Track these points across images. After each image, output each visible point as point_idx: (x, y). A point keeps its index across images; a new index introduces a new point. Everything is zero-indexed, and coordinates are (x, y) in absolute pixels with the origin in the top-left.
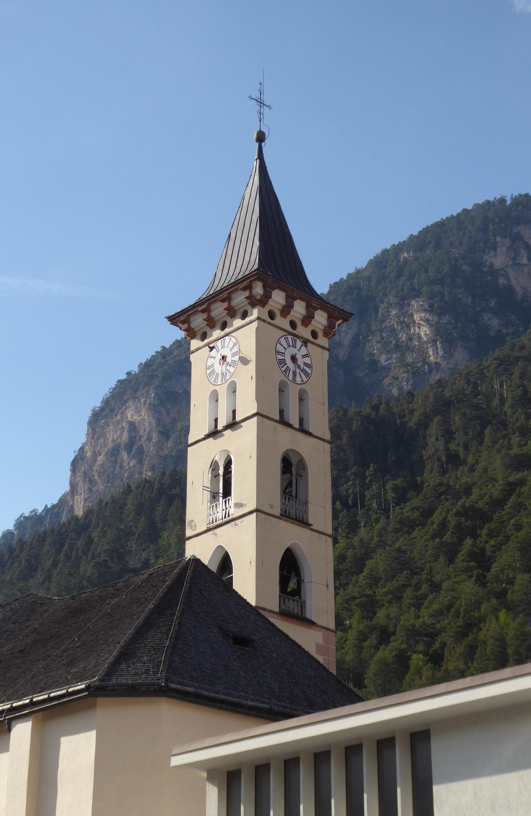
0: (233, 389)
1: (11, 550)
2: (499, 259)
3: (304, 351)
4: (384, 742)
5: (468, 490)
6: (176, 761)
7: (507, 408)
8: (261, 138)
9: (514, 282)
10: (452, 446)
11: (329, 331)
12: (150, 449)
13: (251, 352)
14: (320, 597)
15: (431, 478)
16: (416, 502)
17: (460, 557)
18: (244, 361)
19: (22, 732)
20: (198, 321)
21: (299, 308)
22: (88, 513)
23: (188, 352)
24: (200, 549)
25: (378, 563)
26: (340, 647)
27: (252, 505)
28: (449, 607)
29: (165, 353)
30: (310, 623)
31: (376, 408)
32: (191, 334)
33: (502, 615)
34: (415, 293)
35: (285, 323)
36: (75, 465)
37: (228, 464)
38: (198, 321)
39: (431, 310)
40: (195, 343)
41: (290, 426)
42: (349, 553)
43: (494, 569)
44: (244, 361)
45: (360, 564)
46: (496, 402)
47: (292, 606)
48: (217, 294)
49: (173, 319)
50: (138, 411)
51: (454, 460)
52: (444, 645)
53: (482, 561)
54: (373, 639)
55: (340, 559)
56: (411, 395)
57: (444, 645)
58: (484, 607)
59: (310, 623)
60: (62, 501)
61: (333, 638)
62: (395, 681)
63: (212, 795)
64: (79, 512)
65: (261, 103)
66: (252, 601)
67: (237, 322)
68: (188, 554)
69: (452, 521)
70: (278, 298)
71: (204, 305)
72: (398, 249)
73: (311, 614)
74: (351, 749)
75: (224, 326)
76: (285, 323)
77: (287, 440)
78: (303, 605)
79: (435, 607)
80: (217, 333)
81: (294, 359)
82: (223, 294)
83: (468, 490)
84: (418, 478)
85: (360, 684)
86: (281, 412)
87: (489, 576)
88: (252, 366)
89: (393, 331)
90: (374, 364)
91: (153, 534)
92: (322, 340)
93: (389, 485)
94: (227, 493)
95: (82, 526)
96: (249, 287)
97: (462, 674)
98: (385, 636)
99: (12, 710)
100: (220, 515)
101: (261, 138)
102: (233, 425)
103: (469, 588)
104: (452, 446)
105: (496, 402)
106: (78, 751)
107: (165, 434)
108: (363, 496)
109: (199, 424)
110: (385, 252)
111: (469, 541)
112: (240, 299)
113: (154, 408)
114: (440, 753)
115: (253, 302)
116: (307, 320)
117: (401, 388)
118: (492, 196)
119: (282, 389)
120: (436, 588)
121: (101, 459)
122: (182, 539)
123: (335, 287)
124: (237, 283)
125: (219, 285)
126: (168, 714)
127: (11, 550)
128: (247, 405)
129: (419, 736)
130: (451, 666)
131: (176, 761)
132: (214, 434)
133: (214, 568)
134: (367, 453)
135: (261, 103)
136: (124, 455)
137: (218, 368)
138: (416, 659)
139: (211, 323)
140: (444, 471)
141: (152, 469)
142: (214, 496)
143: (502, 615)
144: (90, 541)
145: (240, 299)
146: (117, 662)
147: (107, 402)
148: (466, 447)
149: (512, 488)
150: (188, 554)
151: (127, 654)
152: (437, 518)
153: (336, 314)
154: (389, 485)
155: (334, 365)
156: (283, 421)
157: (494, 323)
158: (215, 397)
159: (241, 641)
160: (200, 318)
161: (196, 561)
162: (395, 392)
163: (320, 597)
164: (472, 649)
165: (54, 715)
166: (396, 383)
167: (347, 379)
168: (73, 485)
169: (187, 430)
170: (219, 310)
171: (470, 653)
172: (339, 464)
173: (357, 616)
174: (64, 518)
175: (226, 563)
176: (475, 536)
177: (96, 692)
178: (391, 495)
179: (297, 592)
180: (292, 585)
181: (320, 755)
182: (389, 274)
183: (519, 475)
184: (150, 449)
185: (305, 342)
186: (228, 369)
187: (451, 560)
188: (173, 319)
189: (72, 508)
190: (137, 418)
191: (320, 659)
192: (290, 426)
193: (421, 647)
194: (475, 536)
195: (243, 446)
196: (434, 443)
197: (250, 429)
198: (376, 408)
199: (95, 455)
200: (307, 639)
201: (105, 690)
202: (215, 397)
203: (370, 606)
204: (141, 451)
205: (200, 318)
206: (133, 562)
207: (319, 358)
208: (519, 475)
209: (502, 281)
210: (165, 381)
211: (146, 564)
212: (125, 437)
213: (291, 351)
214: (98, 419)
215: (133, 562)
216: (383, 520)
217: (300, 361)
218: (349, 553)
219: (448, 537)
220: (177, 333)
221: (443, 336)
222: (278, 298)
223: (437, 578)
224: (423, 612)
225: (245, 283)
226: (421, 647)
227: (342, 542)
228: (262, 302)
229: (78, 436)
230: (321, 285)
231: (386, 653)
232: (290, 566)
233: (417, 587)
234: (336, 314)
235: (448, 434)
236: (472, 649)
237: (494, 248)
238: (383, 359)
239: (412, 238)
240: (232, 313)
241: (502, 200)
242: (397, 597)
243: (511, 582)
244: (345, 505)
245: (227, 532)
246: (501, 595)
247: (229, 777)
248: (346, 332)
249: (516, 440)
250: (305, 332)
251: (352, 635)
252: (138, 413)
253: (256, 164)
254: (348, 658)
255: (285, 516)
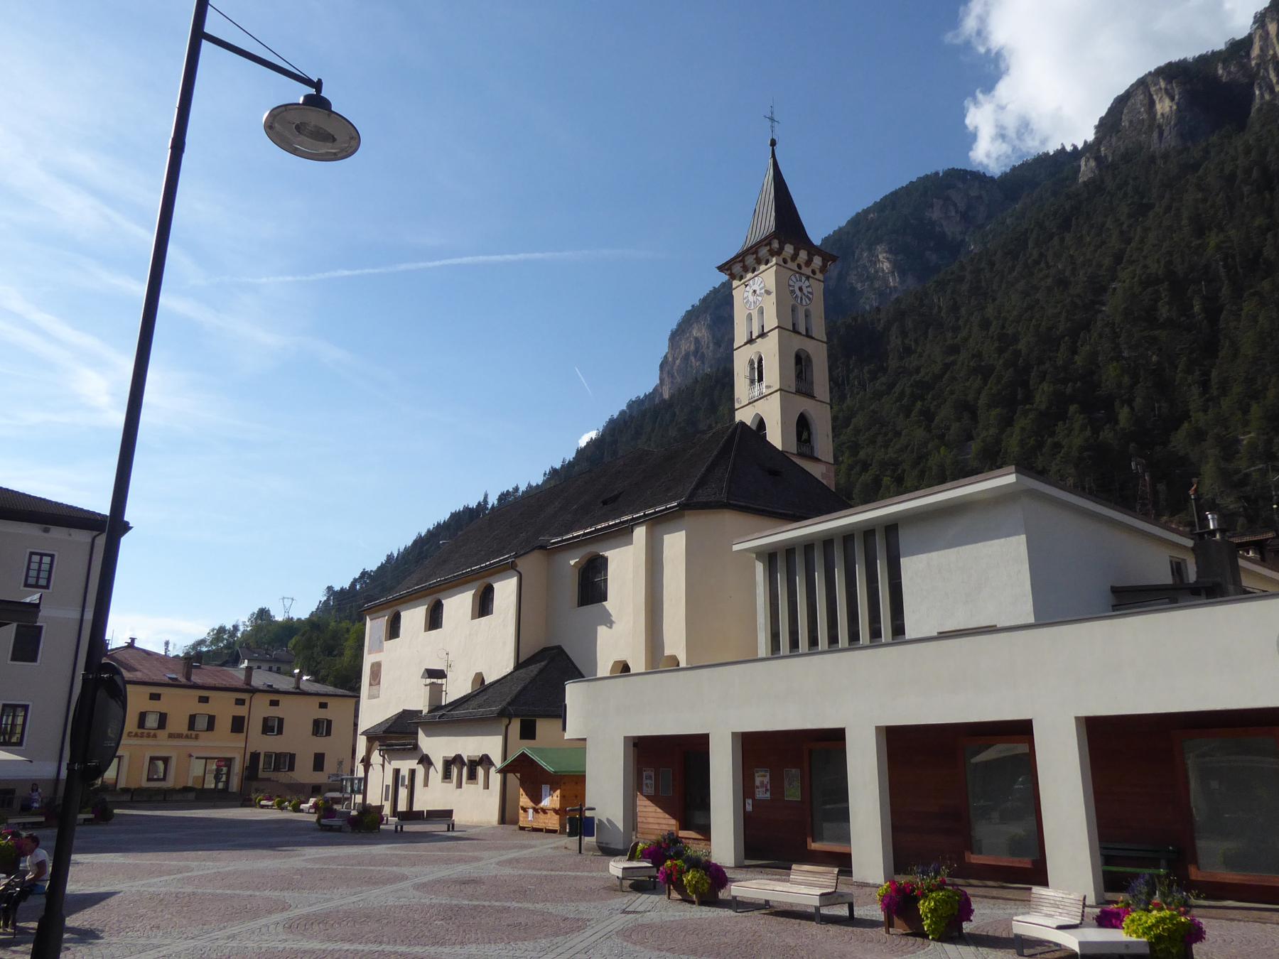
0: (761, 311)
1: (625, 422)
2: (935, 214)
3: (807, 283)
4: (868, 532)
5: (918, 370)
6: (735, 548)
7: (942, 314)
8: (773, 143)
9: (946, 230)
10: (907, 341)
11: (823, 269)
12: (709, 353)
13: (773, 288)
14: (824, 443)
15: (893, 363)
16: (883, 379)
17: (913, 414)
18: (768, 293)
19: (640, 533)
20: (737, 269)
21: (803, 255)
22: (672, 397)
23: (731, 289)
24: (744, 416)
25: (859, 420)
26: (837, 474)
27: (778, 387)
28: (907, 447)
29: (715, 291)
30: (817, 460)
31: (855, 319)
32: (733, 277)
33: (942, 450)
34: (879, 241)
35: (794, 266)
36: (662, 366)
37: (760, 360)
38: (737, 269)
39: (890, 251)
40: (735, 283)
41: (799, 333)
42: (841, 415)
43: (937, 419)
44: (768, 293)
45: (847, 422)
46: (935, 310)
47: (805, 449)
48: (748, 250)
49: (721, 268)
50: (700, 330)
51: (908, 351)
52: (904, 471)
53: (928, 416)
54: (858, 468)
55: (834, 419)
56: (878, 310)
57: (904, 471)
58: (930, 446)
59: (817, 460)
60: (655, 390)
61: (833, 468)
62: (873, 495)
63: (760, 568)
64: (666, 396)
65: (772, 120)
66: (780, 448)
67: (763, 267)
68: (737, 419)
69: (908, 391)
70: (789, 249)
71: (740, 258)
72: (867, 212)
73: (818, 454)
74: (847, 537)
75: (754, 271)
76: (794, 266)
77: (798, 343)
78: (812, 448)
79: (898, 447)
80: (750, 275)
81: (801, 289)
82: (753, 250)
83: (918, 370)
84: (36, 805)
85: (850, 498)
86: (794, 325)
87: (933, 426)
88: (774, 295)
89: (865, 267)
90: (853, 290)
91: (713, 408)
92: (819, 276)
93: (866, 369)
94: (760, 379)
95: (668, 405)
96: (770, 244)
97: (917, 489)
98: (865, 466)
99: (633, 519)
100: (756, 393)
101: (773, 143)
102: (763, 335)
103: (920, 433)
104: (907, 341)
105: (935, 310)
106: (675, 543)
107: (718, 344)
108: (848, 377)
109: (740, 336)
110: (858, 214)
111: (919, 404)
112: (764, 251)
113: (710, 328)
114: (905, 537)
115: (772, 253)
116: (809, 263)
117: (871, 306)
118: (929, 171)
119: (794, 309)
120: (898, 434)
121: (678, 362)
122: (732, 411)
123: (825, 240)
124: (761, 241)
125: (749, 244)
126: (729, 520)
127: (625, 422)
128: (771, 321)
129: (891, 528)
130: (909, 485)
131: (735, 548)
132: (751, 341)
133: (754, 427)
134: (851, 348)
135: (772, 120)
136: (692, 359)
137: (751, 298)
138: (886, 480)
139: (746, 269)
140: (901, 358)
141: (711, 367)
142: (752, 382)
143: (942, 450)
144: (675, 414)
145: (764, 251)
146: (696, 488)
147: (679, 325)
148: (916, 341)
149: (947, 367)
150: (737, 419)
151: (702, 483)
152: (897, 389)
153: (828, 258)
154: (866, 369)
155: (826, 292)
156: (795, 330)
157: (933, 257)
158: (750, 317)
159: (774, 473)
160: (739, 266)
161: (742, 424)
162: (868, 307)
163: (824, 443)
164: (922, 473)
165: (658, 523)
166: (868, 302)
167: (836, 302)
168: (661, 380)
169: (733, 340)
170: (750, 260)
171: (921, 476)
172: (832, 358)
173: (847, 454)
174: (657, 401)
175: (761, 424)
176: (923, 399)
177: (685, 507)
178: (867, 376)
179: (808, 441)
180: (805, 436)
181: (827, 541)
182: (864, 229)
183: (952, 358)
184: (709, 353)
185: (808, 278)
186: (757, 298)
187: (908, 416)
188: (721, 268)
189: (661, 394)
190: (699, 335)
191: (825, 482)
192: (799, 333)
193: (889, 472)
194: (923, 399)
195: (770, 349)
196: (895, 341)
197: (774, 337)
198: (855, 319)
199: (674, 359)
200: (816, 470)
201: (691, 505)
202: (750, 317)
203: (855, 448)
204: (703, 355)
205: (739, 266)
206: (702, 426)
207: (817, 288)
208: (952, 358)
209: (938, 229)
210: (717, 309)
211: (710, 427)
212: (692, 347)
213: (799, 284)
214: (675, 337)
215: (702, 426)
216: (862, 393)
217: (805, 291)
218: (841, 415)
219: (905, 401)
220: (724, 277)
221: (897, 267)
222: (789, 249)
223: (898, 429)
224: (890, 450)
225: (766, 241)
226: (889, 472)
227: (836, 408)
228: (778, 253)
229: (663, 348)
230: (816, 240)
231: (867, 477)
232: (803, 426)
233: (886, 434)
234: (828, 258)
235: (904, 334)
236: (922, 473)
237: (932, 206)
238: (859, 286)
239: (876, 203)
240: (759, 262)
241: (937, 173)
242: (872, 442)
243: (948, 429)
244: (837, 384)
245: (761, 404)
246: (942, 437)
247: (770, 557)
248: (834, 269)
249: (950, 334)
250: (807, 271)
251: (843, 468)
252: (700, 331)
253: (771, 161)
254: (842, 481)
255: (799, 392)
